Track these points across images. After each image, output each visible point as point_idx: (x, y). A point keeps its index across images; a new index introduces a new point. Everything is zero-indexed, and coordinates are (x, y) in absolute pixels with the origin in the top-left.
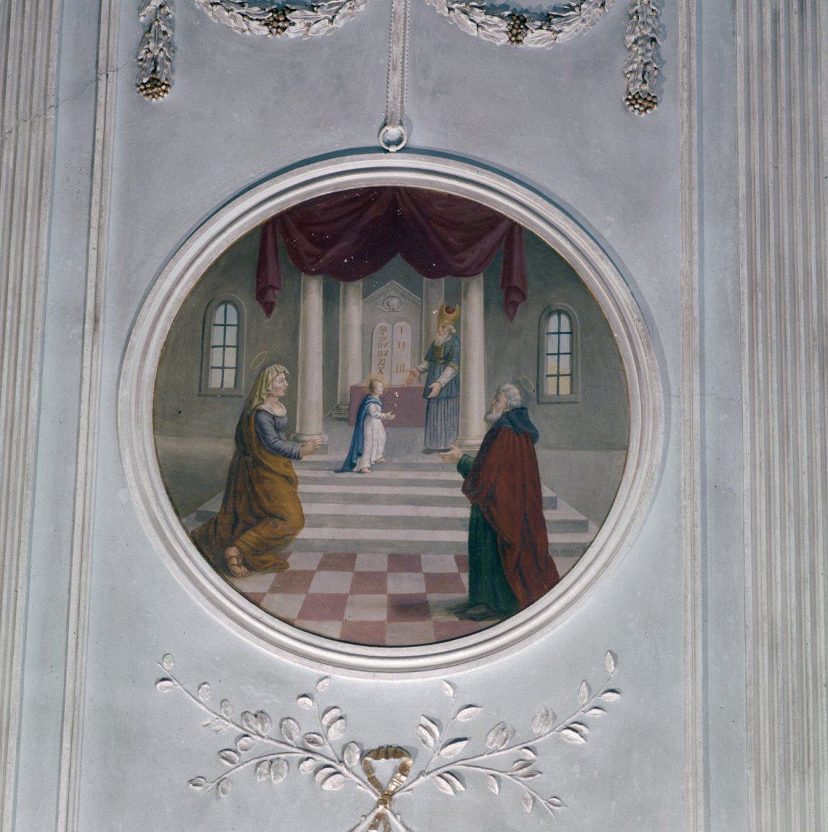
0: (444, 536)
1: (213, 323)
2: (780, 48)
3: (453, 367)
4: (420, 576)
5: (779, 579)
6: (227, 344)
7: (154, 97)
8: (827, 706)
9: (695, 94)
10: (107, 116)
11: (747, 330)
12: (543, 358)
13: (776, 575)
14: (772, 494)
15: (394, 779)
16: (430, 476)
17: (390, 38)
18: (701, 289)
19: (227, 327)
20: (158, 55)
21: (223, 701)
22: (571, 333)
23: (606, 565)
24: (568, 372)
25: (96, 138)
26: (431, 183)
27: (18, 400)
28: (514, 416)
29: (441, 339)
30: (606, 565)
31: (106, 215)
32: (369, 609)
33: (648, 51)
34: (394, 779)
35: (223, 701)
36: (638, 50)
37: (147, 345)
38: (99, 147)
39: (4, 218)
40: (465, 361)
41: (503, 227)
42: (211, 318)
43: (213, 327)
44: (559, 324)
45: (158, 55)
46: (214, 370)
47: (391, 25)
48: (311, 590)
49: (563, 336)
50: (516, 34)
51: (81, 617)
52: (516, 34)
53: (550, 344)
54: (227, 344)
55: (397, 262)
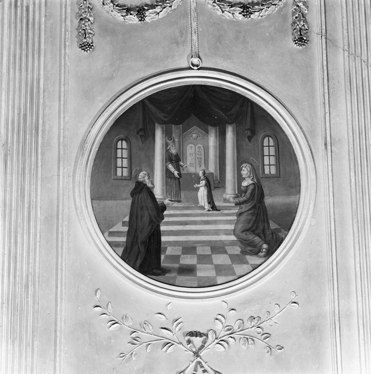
0: (172, 212)
1: (275, 157)
2: (26, 23)
3: (169, 164)
4: (182, 256)
5: (24, 260)
6: (268, 166)
7: (301, 46)
8: (1, 108)
9: (63, 43)
10: (321, 43)
11: (39, 147)
12: (129, 157)
13: (26, 262)
14: (28, 217)
15: (193, 346)
16: (178, 212)
17: (197, 19)
18: (59, 129)
19: (269, 164)
20: (299, 28)
21: (269, 312)
22: (117, 149)
23: (100, 251)
24: (118, 168)
25: (326, 66)
26: (179, 83)
27: (360, 177)
28: (142, 185)
29: (173, 151)
30: (100, 251)
31: (322, 101)
32: (205, 271)
33: (84, 24)
34: (193, 346)
35: (269, 312)
36: (88, 24)
37: (303, 155)
38: (325, 68)
39: (370, 269)
40: (163, 169)
41: (147, 102)
42: (275, 149)
43: (275, 155)
44: (122, 145)
45: (299, 28)
46: (274, 164)
47: (197, 16)
48: (230, 263)
49: (121, 166)
50: (142, 17)
51: (332, 275)
52: (142, 17)
53: (126, 153)
54: (268, 166)
55: (193, 117)
